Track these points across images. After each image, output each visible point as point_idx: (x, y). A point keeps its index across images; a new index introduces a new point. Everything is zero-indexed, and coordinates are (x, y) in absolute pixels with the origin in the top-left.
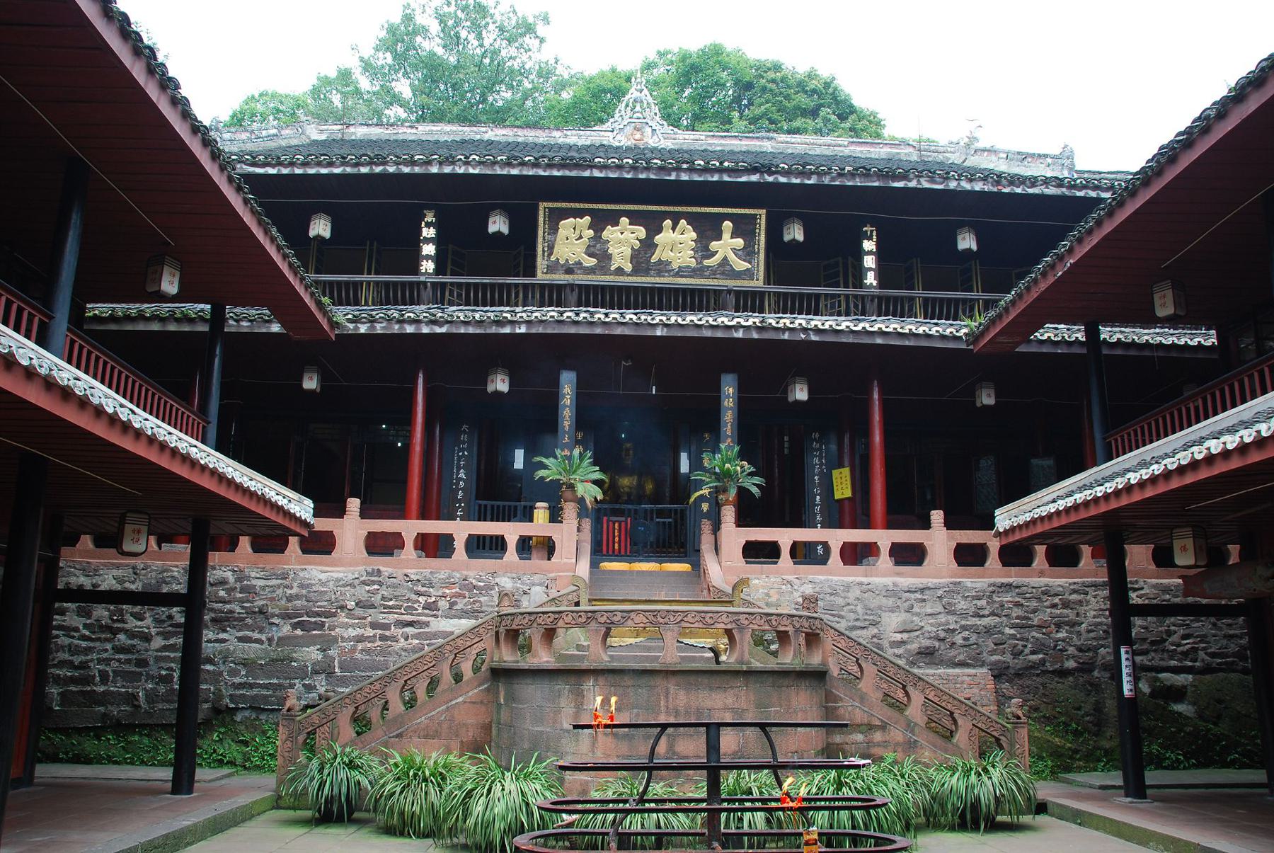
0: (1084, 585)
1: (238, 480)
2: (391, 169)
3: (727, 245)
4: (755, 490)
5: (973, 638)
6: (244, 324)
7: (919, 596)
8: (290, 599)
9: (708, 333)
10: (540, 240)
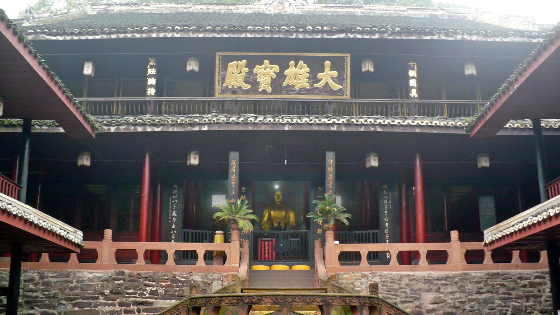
0: (542, 273)
1: (36, 222)
2: (129, 36)
3: (328, 75)
4: (345, 221)
5: (476, 307)
6: (44, 128)
7: (444, 282)
8: (71, 289)
9: (316, 128)
10: (217, 74)
